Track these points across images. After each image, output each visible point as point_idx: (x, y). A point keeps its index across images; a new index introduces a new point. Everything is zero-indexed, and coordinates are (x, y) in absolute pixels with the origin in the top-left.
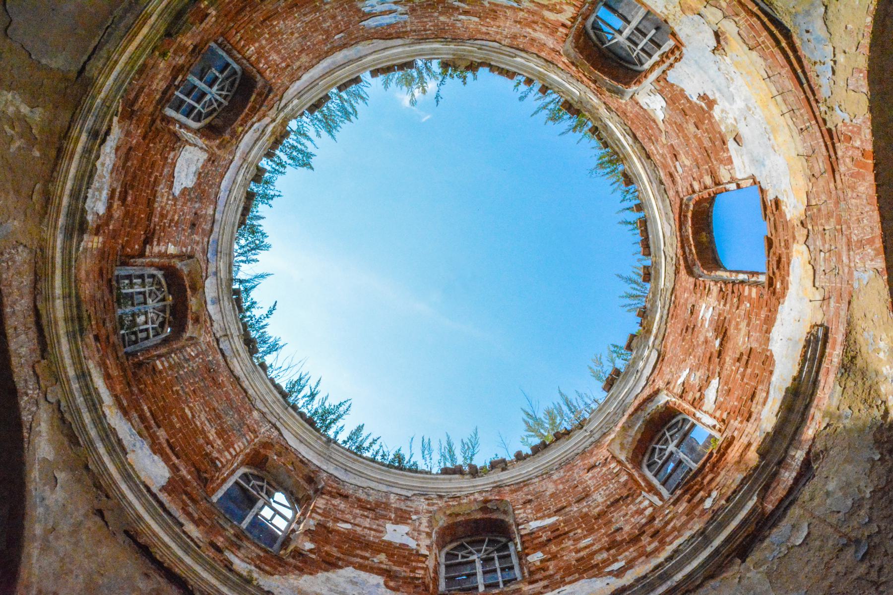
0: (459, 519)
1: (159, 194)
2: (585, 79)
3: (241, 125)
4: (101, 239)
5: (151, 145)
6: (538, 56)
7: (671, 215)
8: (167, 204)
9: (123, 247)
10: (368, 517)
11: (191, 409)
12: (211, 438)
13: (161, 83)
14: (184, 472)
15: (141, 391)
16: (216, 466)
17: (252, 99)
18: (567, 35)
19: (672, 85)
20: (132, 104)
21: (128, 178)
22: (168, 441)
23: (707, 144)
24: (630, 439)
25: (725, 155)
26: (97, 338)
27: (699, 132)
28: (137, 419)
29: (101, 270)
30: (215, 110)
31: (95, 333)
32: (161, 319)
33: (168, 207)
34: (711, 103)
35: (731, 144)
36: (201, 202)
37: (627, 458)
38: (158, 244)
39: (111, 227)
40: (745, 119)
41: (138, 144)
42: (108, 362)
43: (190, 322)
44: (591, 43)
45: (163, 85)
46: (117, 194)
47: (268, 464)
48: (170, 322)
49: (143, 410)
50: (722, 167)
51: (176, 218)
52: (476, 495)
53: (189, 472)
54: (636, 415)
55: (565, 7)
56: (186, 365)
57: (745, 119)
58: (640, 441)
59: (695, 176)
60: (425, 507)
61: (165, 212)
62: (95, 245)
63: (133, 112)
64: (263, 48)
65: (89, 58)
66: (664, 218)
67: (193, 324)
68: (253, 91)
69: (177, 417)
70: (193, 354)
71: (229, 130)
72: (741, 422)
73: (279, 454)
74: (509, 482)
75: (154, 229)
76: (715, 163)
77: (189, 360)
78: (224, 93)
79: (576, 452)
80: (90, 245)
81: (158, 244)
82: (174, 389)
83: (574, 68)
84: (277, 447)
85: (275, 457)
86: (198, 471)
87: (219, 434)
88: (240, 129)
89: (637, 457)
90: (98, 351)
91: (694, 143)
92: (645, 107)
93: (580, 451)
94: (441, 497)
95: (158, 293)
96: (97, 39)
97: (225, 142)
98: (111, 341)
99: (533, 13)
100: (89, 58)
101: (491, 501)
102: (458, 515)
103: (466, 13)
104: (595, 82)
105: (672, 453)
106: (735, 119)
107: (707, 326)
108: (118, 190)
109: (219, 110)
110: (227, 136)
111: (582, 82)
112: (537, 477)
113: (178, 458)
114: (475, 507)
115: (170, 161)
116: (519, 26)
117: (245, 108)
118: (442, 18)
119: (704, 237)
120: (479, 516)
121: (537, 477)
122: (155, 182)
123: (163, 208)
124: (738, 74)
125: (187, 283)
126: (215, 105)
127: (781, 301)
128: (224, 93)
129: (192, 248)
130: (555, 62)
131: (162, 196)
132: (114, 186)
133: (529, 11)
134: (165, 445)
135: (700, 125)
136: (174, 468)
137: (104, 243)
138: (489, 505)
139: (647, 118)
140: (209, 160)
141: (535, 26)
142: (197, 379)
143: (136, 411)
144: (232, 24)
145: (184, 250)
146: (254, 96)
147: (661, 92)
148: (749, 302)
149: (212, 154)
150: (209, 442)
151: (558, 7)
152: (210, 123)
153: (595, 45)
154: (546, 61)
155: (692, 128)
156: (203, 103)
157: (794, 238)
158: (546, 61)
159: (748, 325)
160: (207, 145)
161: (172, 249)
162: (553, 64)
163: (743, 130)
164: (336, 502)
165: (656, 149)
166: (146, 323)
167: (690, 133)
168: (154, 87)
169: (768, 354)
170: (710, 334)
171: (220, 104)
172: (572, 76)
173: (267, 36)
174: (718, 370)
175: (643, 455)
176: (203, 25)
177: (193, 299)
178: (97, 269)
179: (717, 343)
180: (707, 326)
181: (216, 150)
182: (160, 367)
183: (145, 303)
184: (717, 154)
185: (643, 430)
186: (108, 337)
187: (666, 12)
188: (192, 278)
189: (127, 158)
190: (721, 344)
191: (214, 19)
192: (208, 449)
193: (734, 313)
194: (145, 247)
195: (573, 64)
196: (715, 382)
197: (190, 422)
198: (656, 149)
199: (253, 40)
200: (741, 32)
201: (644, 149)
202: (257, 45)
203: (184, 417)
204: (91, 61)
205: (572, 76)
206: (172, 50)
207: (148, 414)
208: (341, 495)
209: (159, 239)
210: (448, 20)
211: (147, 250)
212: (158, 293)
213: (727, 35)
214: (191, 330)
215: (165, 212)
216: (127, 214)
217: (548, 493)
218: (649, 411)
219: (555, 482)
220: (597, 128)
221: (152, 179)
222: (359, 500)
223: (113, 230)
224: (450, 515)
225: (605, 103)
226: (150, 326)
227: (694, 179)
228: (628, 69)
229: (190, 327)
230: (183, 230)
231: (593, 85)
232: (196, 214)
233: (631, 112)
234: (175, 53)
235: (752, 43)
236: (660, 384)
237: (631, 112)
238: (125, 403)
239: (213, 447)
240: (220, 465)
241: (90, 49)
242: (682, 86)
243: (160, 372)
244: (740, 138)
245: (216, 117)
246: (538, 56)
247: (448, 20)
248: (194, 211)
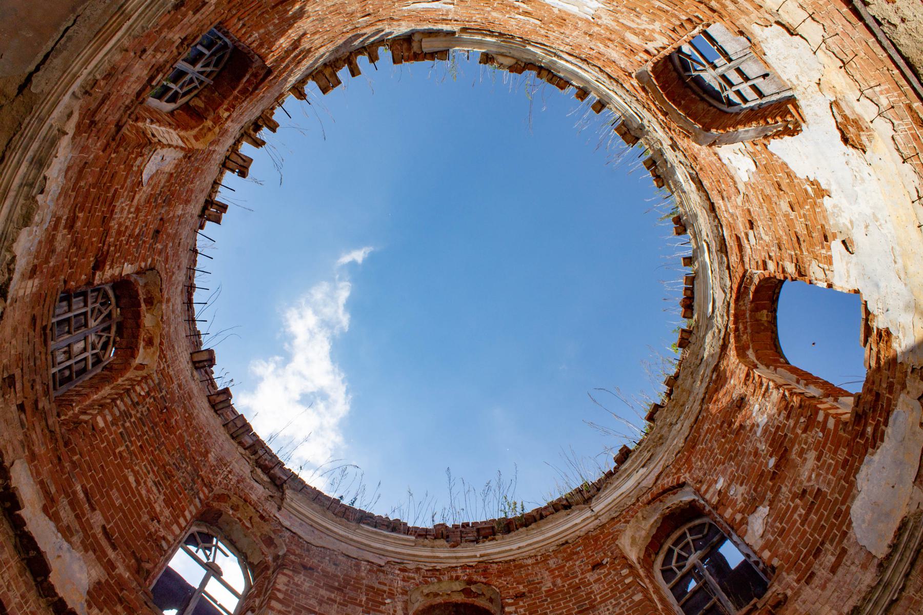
0: (439, 600)
1: (117, 210)
2: (653, 107)
3: (227, 110)
4: (37, 281)
5: (113, 156)
6: (601, 70)
7: (728, 283)
8: (127, 218)
9: (65, 282)
10: (335, 601)
11: (136, 474)
12: (158, 509)
13: (134, 86)
14: (121, 570)
15: (74, 465)
16: (160, 547)
17: (245, 80)
18: (646, 61)
19: (772, 154)
20: (93, 115)
21: (80, 199)
22: (104, 527)
23: (800, 229)
24: (643, 533)
25: (824, 251)
26: (21, 408)
27: (793, 215)
28: (68, 507)
29: (34, 319)
30: (196, 88)
31: (19, 402)
32: (104, 339)
33: (128, 223)
34: (822, 192)
35: (836, 246)
36: (169, 204)
37: (639, 558)
38: (111, 267)
39: (51, 264)
40: (867, 227)
41: (97, 158)
42: (34, 436)
43: (142, 344)
44: (671, 67)
45: (137, 87)
46: (63, 221)
47: (220, 520)
48: (114, 342)
49: (75, 493)
50: (814, 263)
51: (137, 231)
52: (459, 572)
53: (128, 567)
54: (653, 505)
55: (656, 36)
56: (133, 412)
57: (867, 227)
58: (654, 537)
59: (772, 254)
60: (401, 583)
61: (123, 229)
62: (28, 291)
63: (93, 123)
64: (270, 32)
65: (37, 69)
66: (585, 66)
67: (144, 348)
68: (246, 71)
69: (118, 490)
70: (143, 393)
71: (212, 115)
72: (798, 581)
73: (235, 508)
74: (498, 558)
75: (108, 251)
76: (805, 253)
77: (138, 403)
78: (208, 69)
79: (577, 533)
80: (21, 293)
81: (111, 267)
82: (117, 451)
83: (643, 94)
84: (234, 499)
85: (231, 512)
86: (139, 561)
87: (168, 503)
88: (226, 114)
89: (650, 556)
90: (22, 425)
91: (781, 222)
92: (725, 161)
93: (582, 534)
94: (418, 570)
95: (103, 309)
96: (51, 44)
97: (205, 130)
98: (40, 406)
99: (612, 32)
100: (37, 69)
101: (476, 583)
102: (436, 595)
103: (526, 13)
104: (665, 114)
105: (694, 567)
106: (851, 222)
107: (758, 434)
108: (65, 217)
109: (200, 88)
110: (209, 123)
111: (649, 110)
112: (530, 557)
113: (114, 548)
114: (457, 586)
115: (135, 169)
116: (588, 38)
117: (234, 89)
118: (494, 14)
119: (764, 315)
120: (460, 598)
121: (530, 557)
122: (114, 196)
123: (120, 225)
124: (874, 177)
125: (142, 297)
126: (196, 83)
127: (870, 450)
128: (208, 69)
129: (153, 259)
130: (620, 81)
131: (122, 210)
132: (59, 213)
133: (607, 28)
134: (100, 536)
135: (796, 207)
136: (110, 566)
137: (41, 284)
138: (473, 588)
139: (725, 174)
140: (185, 157)
141: (609, 44)
142: (146, 429)
143: (67, 496)
144: (234, 12)
145: (143, 264)
146: (247, 76)
147: (753, 155)
148: (823, 431)
149: (190, 150)
150: (155, 517)
151: (647, 33)
152: (187, 103)
153: (676, 70)
154: (610, 77)
155: (785, 207)
156: (180, 84)
157: (904, 386)
158: (610, 77)
159: (818, 459)
160: (182, 138)
161: (128, 269)
162: (617, 82)
163: (858, 236)
164: (300, 578)
165: (726, 206)
166: (85, 350)
167: (781, 210)
168: (123, 92)
169: (844, 508)
170: (763, 447)
171: (201, 83)
172: (637, 100)
173: (277, 22)
174: (769, 495)
175: (657, 554)
176: (198, 15)
177: (148, 315)
178: (27, 320)
179: (772, 462)
180: (758, 434)
181: (193, 141)
182: (101, 424)
183: (86, 325)
184: (812, 245)
185: (659, 525)
186: (36, 402)
187: (795, 82)
188: (149, 292)
189: (80, 174)
190: (777, 466)
191: (212, 8)
192: (154, 526)
193: (797, 435)
194: (94, 274)
195: (644, 89)
196: (763, 510)
197: (133, 492)
198: (726, 206)
199: (257, 26)
200: (897, 137)
201: (709, 199)
202: (262, 31)
203: (126, 489)
204: (40, 73)
205: (637, 100)
206: (153, 48)
207: (81, 495)
208: (305, 567)
209: (112, 262)
210: (500, 17)
211: (97, 277)
212: (103, 309)
213: (876, 134)
214: (142, 356)
215: (123, 229)
216: (75, 243)
217: (544, 589)
218: (669, 504)
219: (552, 571)
220: (654, 163)
221: (110, 195)
222: (326, 574)
223: (54, 266)
224: (428, 595)
225: (671, 139)
226: (88, 354)
227: (770, 257)
228: (711, 105)
229: (141, 350)
230: (144, 242)
231: (662, 117)
232: (162, 219)
233: (704, 159)
234: (156, 50)
235: (907, 152)
236: (685, 476)
237: (704, 159)
238: (53, 490)
239: (159, 522)
240: (166, 547)
241: (40, 57)
242: (786, 159)
243: (102, 431)
244: (852, 242)
245: (196, 96)
246: (601, 70)
247: (500, 17)
248: (159, 217)
